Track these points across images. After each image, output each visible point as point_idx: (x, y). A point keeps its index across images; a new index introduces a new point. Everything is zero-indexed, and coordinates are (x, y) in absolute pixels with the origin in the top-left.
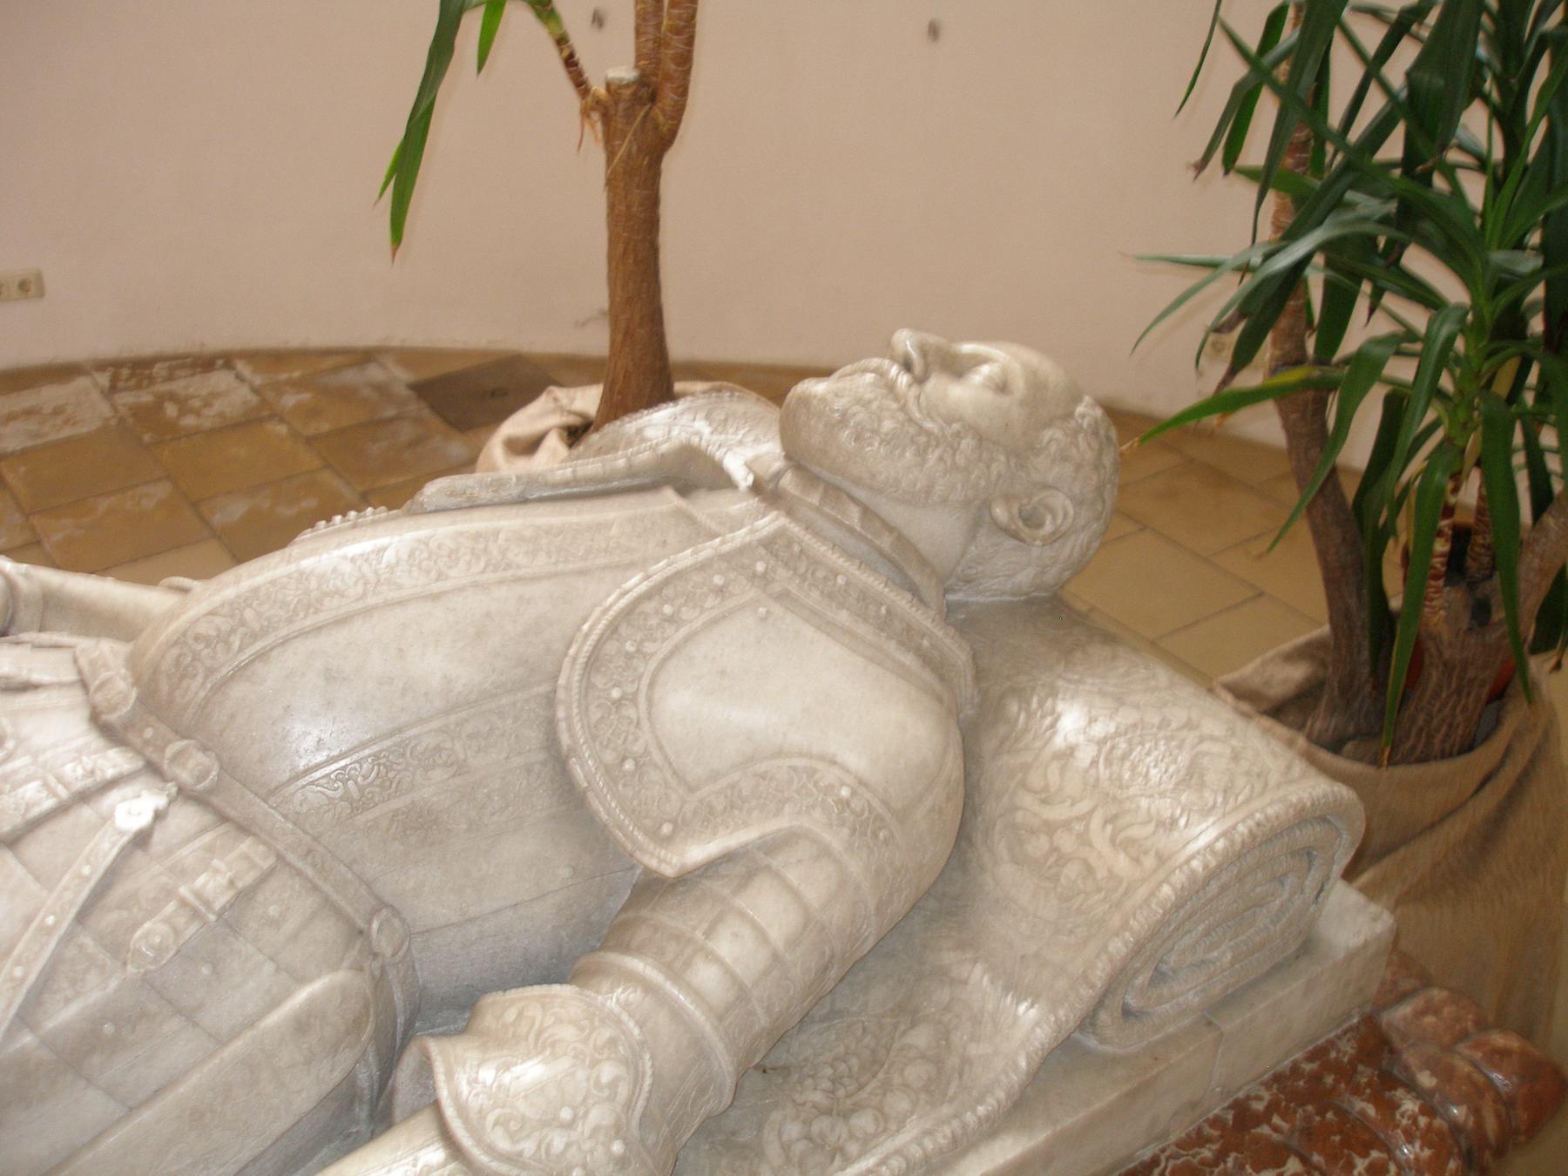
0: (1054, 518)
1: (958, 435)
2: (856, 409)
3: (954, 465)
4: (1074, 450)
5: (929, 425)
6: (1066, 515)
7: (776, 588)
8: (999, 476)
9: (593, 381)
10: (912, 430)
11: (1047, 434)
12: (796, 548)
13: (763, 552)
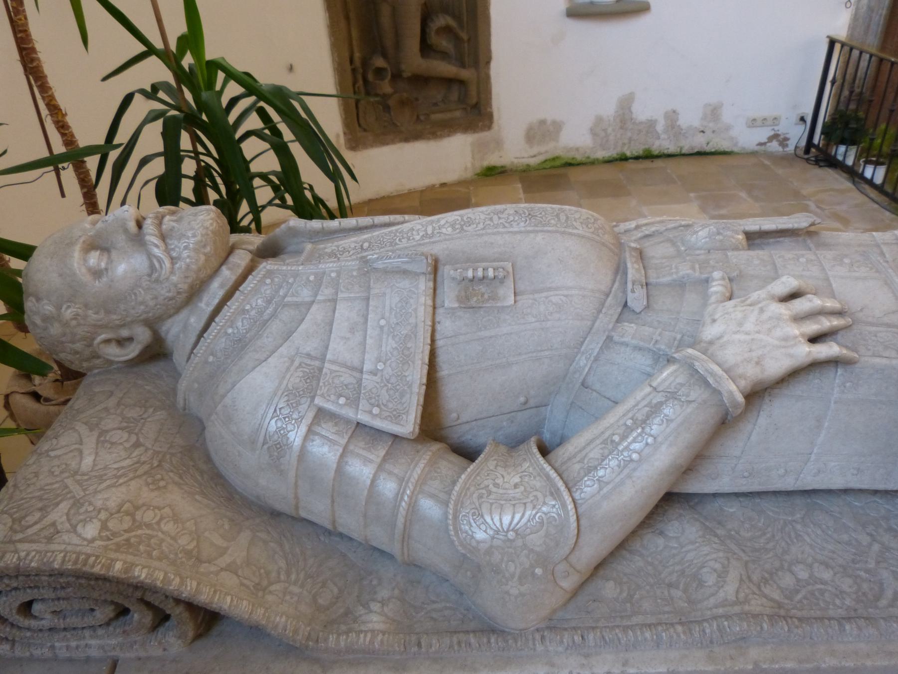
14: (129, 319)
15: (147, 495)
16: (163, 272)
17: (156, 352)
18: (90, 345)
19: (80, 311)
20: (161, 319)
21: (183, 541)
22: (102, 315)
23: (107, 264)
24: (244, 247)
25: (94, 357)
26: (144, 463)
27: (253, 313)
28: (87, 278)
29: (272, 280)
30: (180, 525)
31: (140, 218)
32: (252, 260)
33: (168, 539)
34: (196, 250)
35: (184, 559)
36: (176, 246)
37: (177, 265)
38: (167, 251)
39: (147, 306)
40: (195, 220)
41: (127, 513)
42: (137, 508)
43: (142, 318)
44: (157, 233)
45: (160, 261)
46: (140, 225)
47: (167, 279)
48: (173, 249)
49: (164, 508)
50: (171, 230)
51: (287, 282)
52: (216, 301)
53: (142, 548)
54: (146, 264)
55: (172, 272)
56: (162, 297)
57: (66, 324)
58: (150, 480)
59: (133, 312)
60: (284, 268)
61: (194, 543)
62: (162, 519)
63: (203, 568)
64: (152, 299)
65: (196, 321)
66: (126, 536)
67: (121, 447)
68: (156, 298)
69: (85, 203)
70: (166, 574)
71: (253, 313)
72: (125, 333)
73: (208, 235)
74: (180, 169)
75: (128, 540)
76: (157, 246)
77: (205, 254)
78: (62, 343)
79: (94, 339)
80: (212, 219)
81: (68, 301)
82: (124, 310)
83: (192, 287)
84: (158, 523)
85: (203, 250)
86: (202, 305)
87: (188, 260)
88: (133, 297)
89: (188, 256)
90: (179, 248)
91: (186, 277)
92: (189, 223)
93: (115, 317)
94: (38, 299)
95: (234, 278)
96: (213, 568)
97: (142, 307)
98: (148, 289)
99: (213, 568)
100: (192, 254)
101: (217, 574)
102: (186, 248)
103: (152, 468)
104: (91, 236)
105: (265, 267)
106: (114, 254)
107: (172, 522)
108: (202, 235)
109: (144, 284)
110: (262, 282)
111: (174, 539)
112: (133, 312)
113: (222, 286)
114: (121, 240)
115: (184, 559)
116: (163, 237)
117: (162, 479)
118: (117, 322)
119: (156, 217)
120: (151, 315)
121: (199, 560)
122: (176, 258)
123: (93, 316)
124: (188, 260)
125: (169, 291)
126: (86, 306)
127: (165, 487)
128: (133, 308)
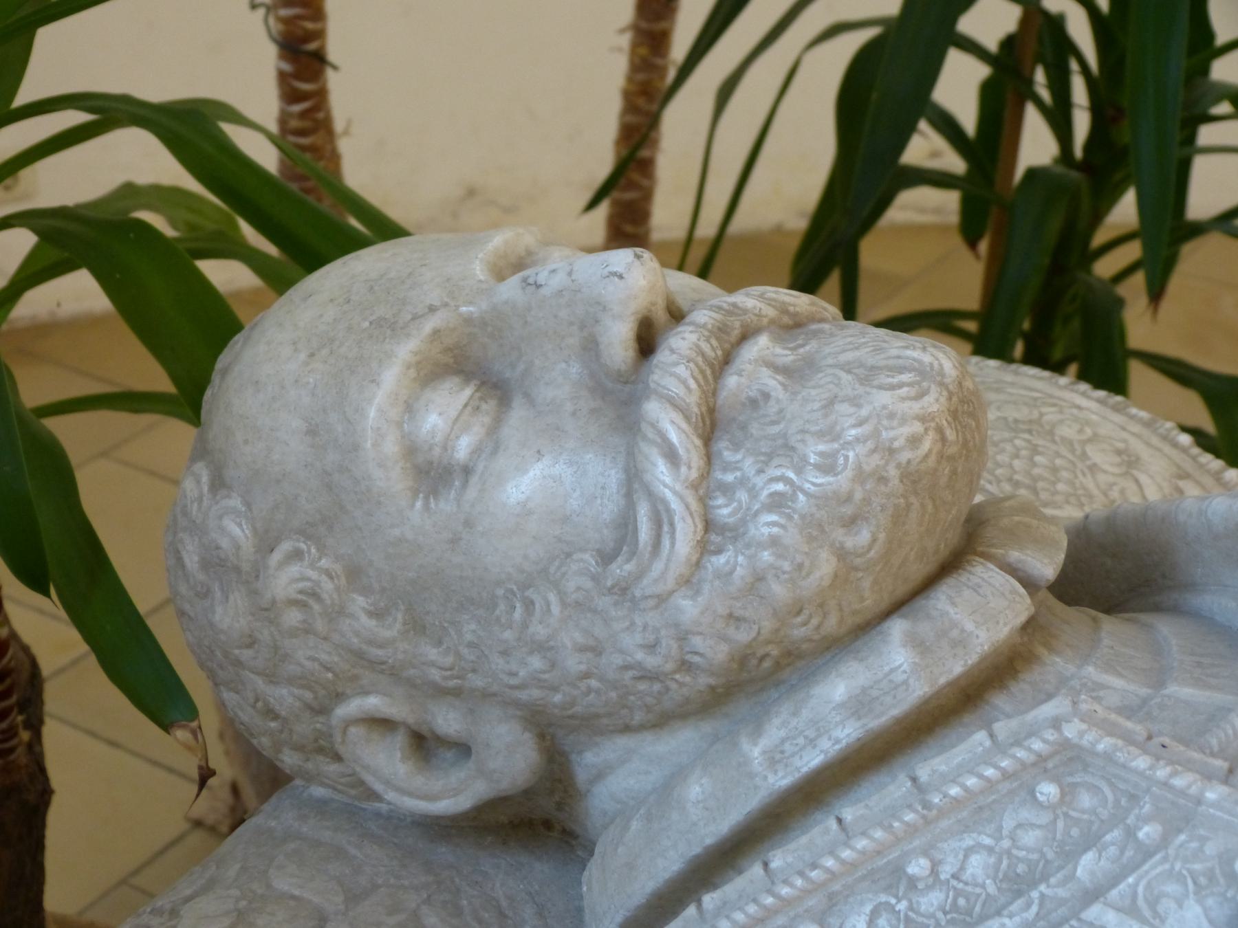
14: (477, 681)
16: (658, 567)
17: (540, 822)
18: (322, 710)
19: (327, 585)
20: (593, 725)
22: (390, 630)
23: (477, 451)
24: (1014, 555)
25: (320, 750)
27: (931, 901)
28: (385, 472)
29: (1068, 793)
31: (660, 315)
32: (1030, 626)
34: (814, 530)
36: (743, 482)
37: (721, 560)
38: (705, 488)
39: (553, 665)
40: (855, 402)
43: (523, 695)
44: (693, 400)
45: (662, 518)
46: (647, 342)
47: (662, 600)
48: (727, 490)
50: (754, 403)
51: (1130, 833)
52: (812, 761)
54: (610, 507)
55: (689, 581)
56: (618, 660)
57: (267, 611)
59: (498, 663)
60: (1142, 762)
64: (582, 649)
65: (709, 808)
68: (596, 650)
69: (636, 28)
71: (931, 901)
72: (447, 720)
73: (883, 480)
74: (954, 21)
76: (672, 456)
77: (842, 554)
78: (238, 663)
79: (340, 697)
80: (922, 419)
81: (305, 533)
82: (471, 645)
83: (743, 659)
85: (839, 534)
86: (755, 752)
87: (766, 556)
88: (518, 614)
89: (774, 542)
90: (753, 493)
91: (733, 618)
92: (830, 403)
93: (432, 653)
94: (219, 484)
95: (919, 690)
97: (536, 662)
98: (578, 604)
100: (792, 537)
102: (777, 503)
104: (468, 321)
105: (1056, 723)
106: (518, 413)
108: (860, 476)
109: (571, 585)
110: (1019, 785)
112: (498, 663)
113: (858, 705)
114: (559, 381)
116: (711, 426)
118: (435, 675)
119: (720, 331)
120: (558, 698)
122: (723, 529)
123: (359, 621)
124: (766, 556)
125: (651, 648)
126: (355, 575)
128: (505, 653)
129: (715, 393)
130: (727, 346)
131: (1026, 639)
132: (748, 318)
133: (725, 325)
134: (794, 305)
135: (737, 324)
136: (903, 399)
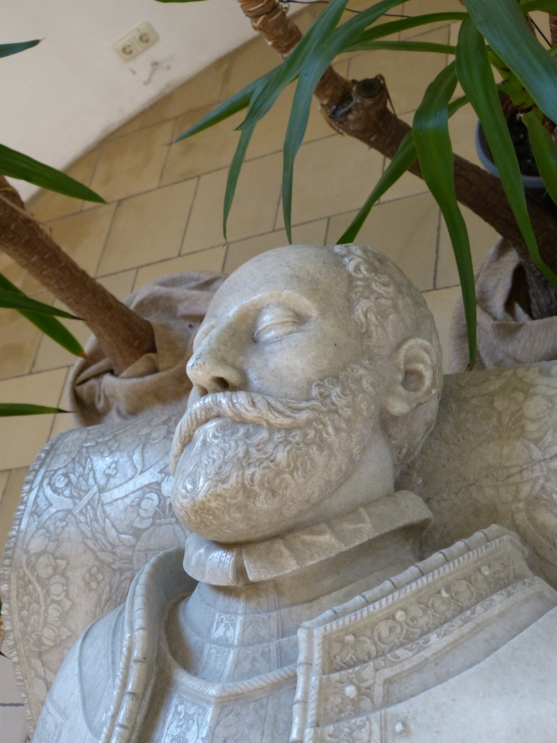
0: (423, 362)
1: (323, 397)
2: (249, 472)
3: (348, 421)
4: (383, 301)
5: (303, 416)
6: (427, 351)
7: (378, 691)
8: (373, 385)
9: (460, 19)
10: (297, 437)
11: (359, 313)
12: (350, 638)
13: (336, 676)
15: (77, 577)
21: (48, 633)
26: (114, 554)
30: (60, 623)
33: (42, 618)
35: (32, 641)
41: (55, 569)
42: (63, 574)
49: (69, 599)
53: (26, 599)
58: (95, 570)
61: (52, 644)
62: (58, 603)
63: (36, 662)
66: (33, 579)
67: (135, 515)
70: (12, 630)
75: (30, 582)
84: (53, 601)
96: (41, 670)
99: (41, 670)
101: (38, 676)
103: (109, 565)
107: (58, 614)
111: (45, 623)
115: (32, 641)
117: (99, 583)
121: (40, 655)
127: (91, 589)
129: (194, 431)
130: (208, 416)
131: (243, 588)
132: (221, 411)
133: (212, 408)
134: (244, 415)
135: (216, 410)
136: (125, 563)
